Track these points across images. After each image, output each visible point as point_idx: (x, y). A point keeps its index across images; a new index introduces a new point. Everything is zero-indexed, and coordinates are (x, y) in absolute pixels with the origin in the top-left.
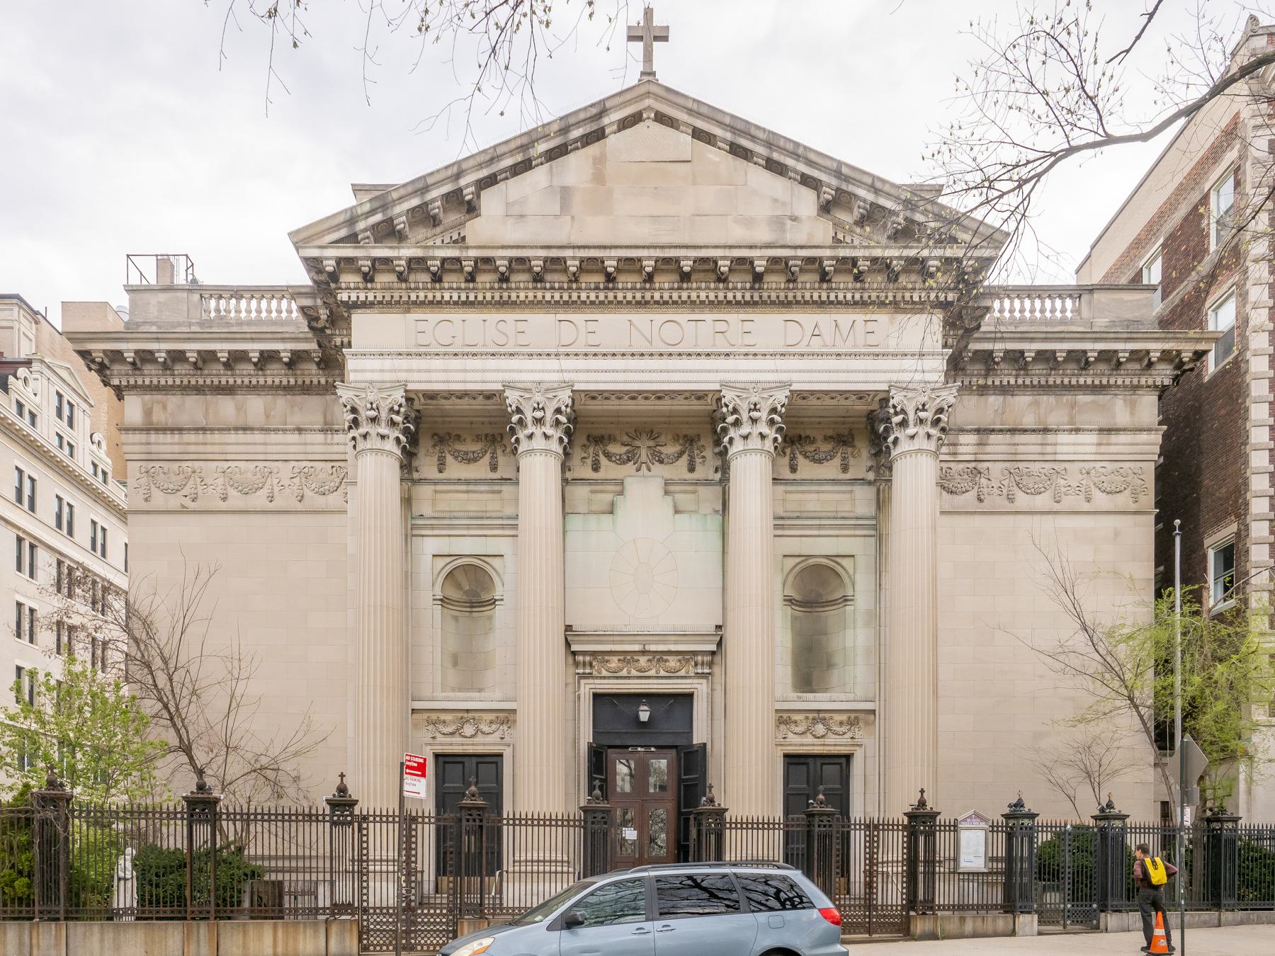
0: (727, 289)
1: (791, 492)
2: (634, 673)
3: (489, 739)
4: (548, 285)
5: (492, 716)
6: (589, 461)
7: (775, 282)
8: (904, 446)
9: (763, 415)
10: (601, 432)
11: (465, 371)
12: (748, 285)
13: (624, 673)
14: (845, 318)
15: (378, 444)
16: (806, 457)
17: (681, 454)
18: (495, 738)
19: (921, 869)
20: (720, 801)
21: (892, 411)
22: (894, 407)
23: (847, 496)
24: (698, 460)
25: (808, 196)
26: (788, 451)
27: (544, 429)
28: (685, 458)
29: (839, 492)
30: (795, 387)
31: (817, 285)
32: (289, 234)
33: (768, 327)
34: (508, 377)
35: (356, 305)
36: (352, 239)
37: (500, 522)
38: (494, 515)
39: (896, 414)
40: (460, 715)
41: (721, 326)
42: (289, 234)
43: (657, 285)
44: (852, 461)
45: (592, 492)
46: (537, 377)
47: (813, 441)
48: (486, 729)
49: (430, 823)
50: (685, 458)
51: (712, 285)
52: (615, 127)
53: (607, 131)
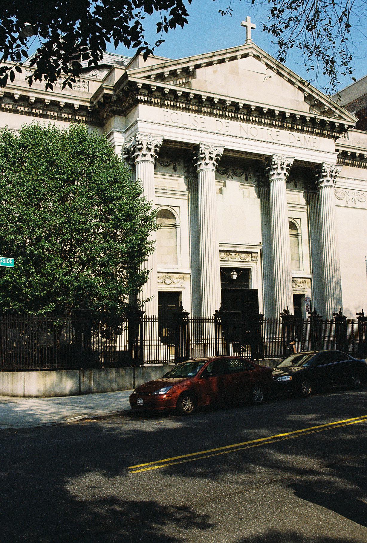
2: (230, 259)
3: (176, 285)
5: (177, 275)
8: (203, 167)
9: (285, 166)
10: (232, 164)
11: (184, 134)
13: (226, 259)
14: (307, 136)
15: (278, 177)
18: (178, 285)
22: (274, 162)
23: (297, 196)
24: (249, 177)
25: (301, 94)
27: (205, 161)
30: (165, 138)
33: (285, 135)
34: (325, 160)
35: (141, 101)
36: (149, 77)
37: (179, 193)
38: (166, 188)
40: (164, 274)
41: (270, 132)
46: (149, 131)
48: (175, 281)
49: (156, 322)
52: (240, 56)
53: (238, 57)
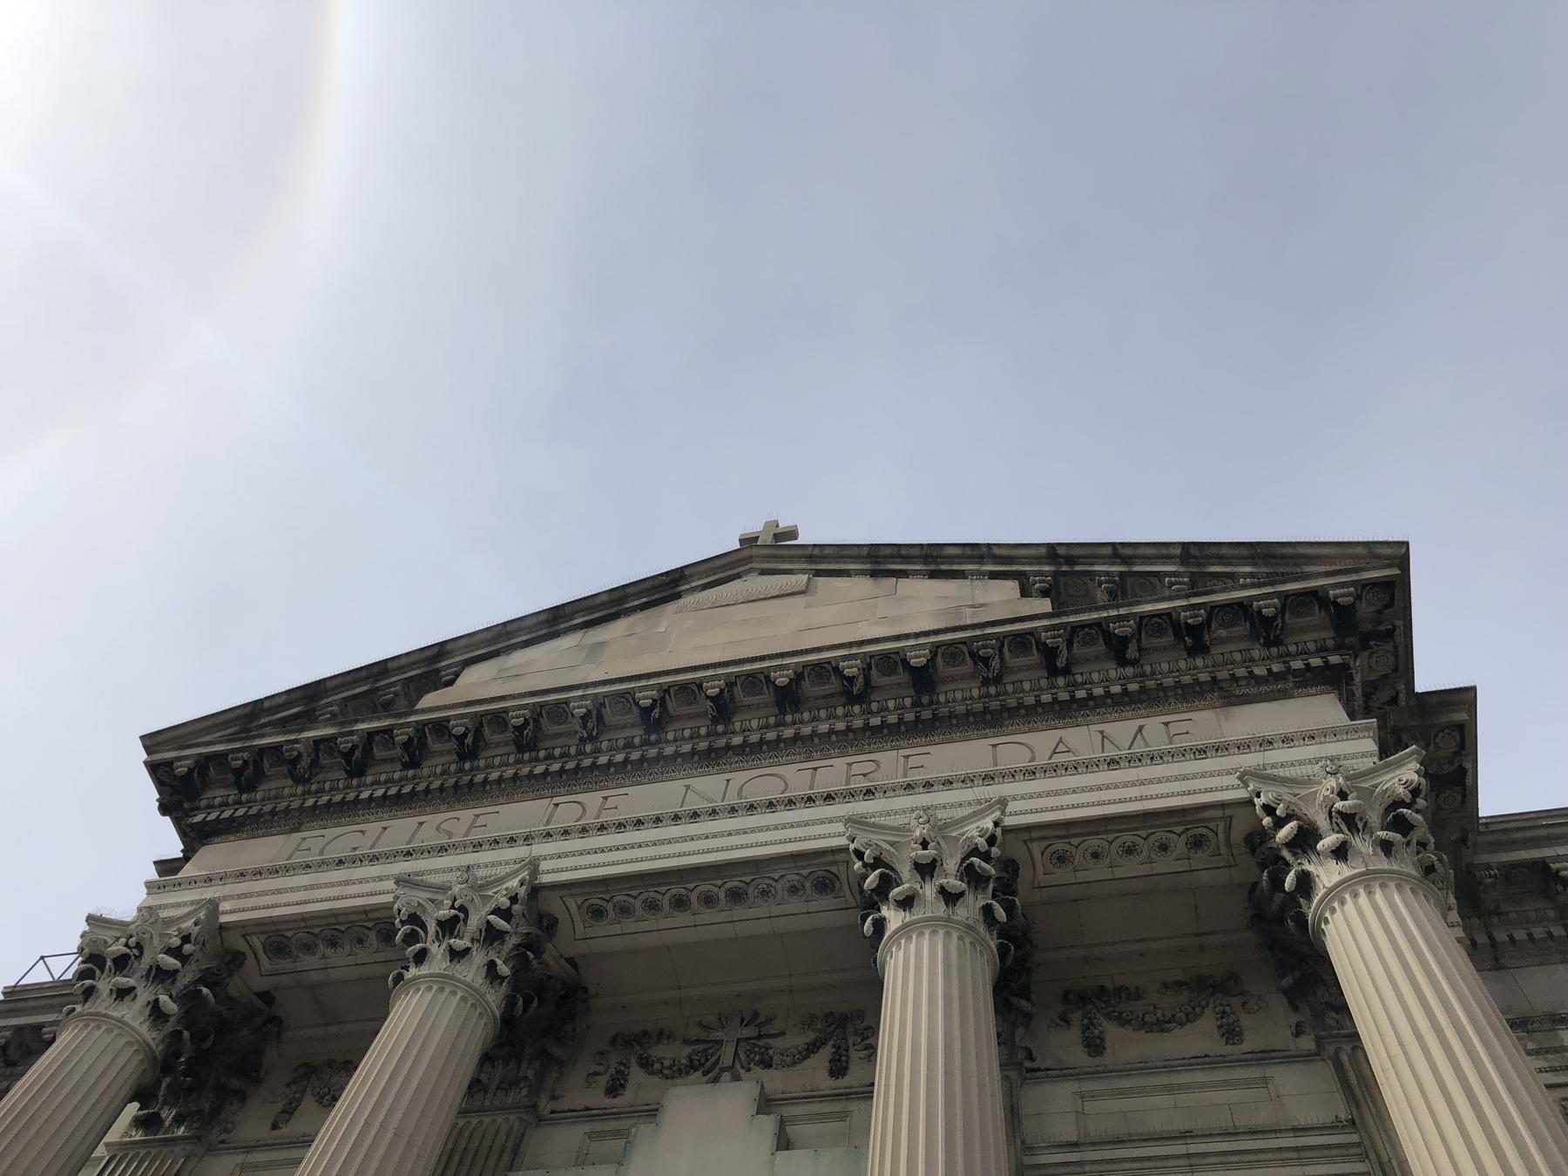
0: (870, 712)
1: (1093, 1096)
4: (542, 754)
6: (603, 1081)
7: (960, 692)
12: (908, 701)
16: (1123, 1021)
17: (812, 1048)
19: (1064, 568)
20: (168, 818)
21: (1267, 821)
26: (1076, 1017)
28: (826, 1052)
29: (1228, 1085)
31: (1044, 682)
32: (142, 738)
39: (1279, 823)
42: (142, 738)
43: (737, 726)
44: (1246, 1021)
45: (593, 1136)
47: (1138, 994)
50: (826, 1052)
51: (840, 711)
